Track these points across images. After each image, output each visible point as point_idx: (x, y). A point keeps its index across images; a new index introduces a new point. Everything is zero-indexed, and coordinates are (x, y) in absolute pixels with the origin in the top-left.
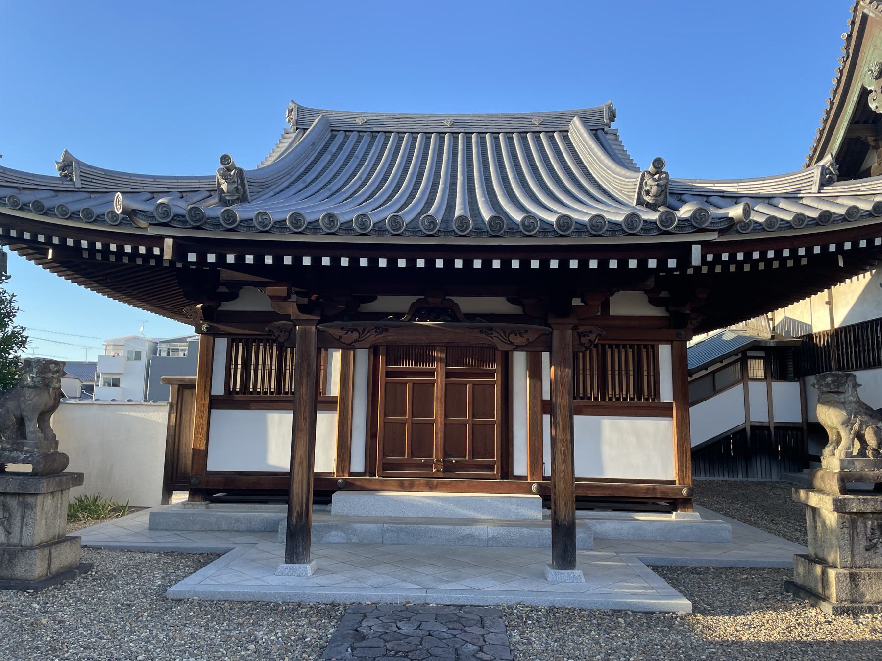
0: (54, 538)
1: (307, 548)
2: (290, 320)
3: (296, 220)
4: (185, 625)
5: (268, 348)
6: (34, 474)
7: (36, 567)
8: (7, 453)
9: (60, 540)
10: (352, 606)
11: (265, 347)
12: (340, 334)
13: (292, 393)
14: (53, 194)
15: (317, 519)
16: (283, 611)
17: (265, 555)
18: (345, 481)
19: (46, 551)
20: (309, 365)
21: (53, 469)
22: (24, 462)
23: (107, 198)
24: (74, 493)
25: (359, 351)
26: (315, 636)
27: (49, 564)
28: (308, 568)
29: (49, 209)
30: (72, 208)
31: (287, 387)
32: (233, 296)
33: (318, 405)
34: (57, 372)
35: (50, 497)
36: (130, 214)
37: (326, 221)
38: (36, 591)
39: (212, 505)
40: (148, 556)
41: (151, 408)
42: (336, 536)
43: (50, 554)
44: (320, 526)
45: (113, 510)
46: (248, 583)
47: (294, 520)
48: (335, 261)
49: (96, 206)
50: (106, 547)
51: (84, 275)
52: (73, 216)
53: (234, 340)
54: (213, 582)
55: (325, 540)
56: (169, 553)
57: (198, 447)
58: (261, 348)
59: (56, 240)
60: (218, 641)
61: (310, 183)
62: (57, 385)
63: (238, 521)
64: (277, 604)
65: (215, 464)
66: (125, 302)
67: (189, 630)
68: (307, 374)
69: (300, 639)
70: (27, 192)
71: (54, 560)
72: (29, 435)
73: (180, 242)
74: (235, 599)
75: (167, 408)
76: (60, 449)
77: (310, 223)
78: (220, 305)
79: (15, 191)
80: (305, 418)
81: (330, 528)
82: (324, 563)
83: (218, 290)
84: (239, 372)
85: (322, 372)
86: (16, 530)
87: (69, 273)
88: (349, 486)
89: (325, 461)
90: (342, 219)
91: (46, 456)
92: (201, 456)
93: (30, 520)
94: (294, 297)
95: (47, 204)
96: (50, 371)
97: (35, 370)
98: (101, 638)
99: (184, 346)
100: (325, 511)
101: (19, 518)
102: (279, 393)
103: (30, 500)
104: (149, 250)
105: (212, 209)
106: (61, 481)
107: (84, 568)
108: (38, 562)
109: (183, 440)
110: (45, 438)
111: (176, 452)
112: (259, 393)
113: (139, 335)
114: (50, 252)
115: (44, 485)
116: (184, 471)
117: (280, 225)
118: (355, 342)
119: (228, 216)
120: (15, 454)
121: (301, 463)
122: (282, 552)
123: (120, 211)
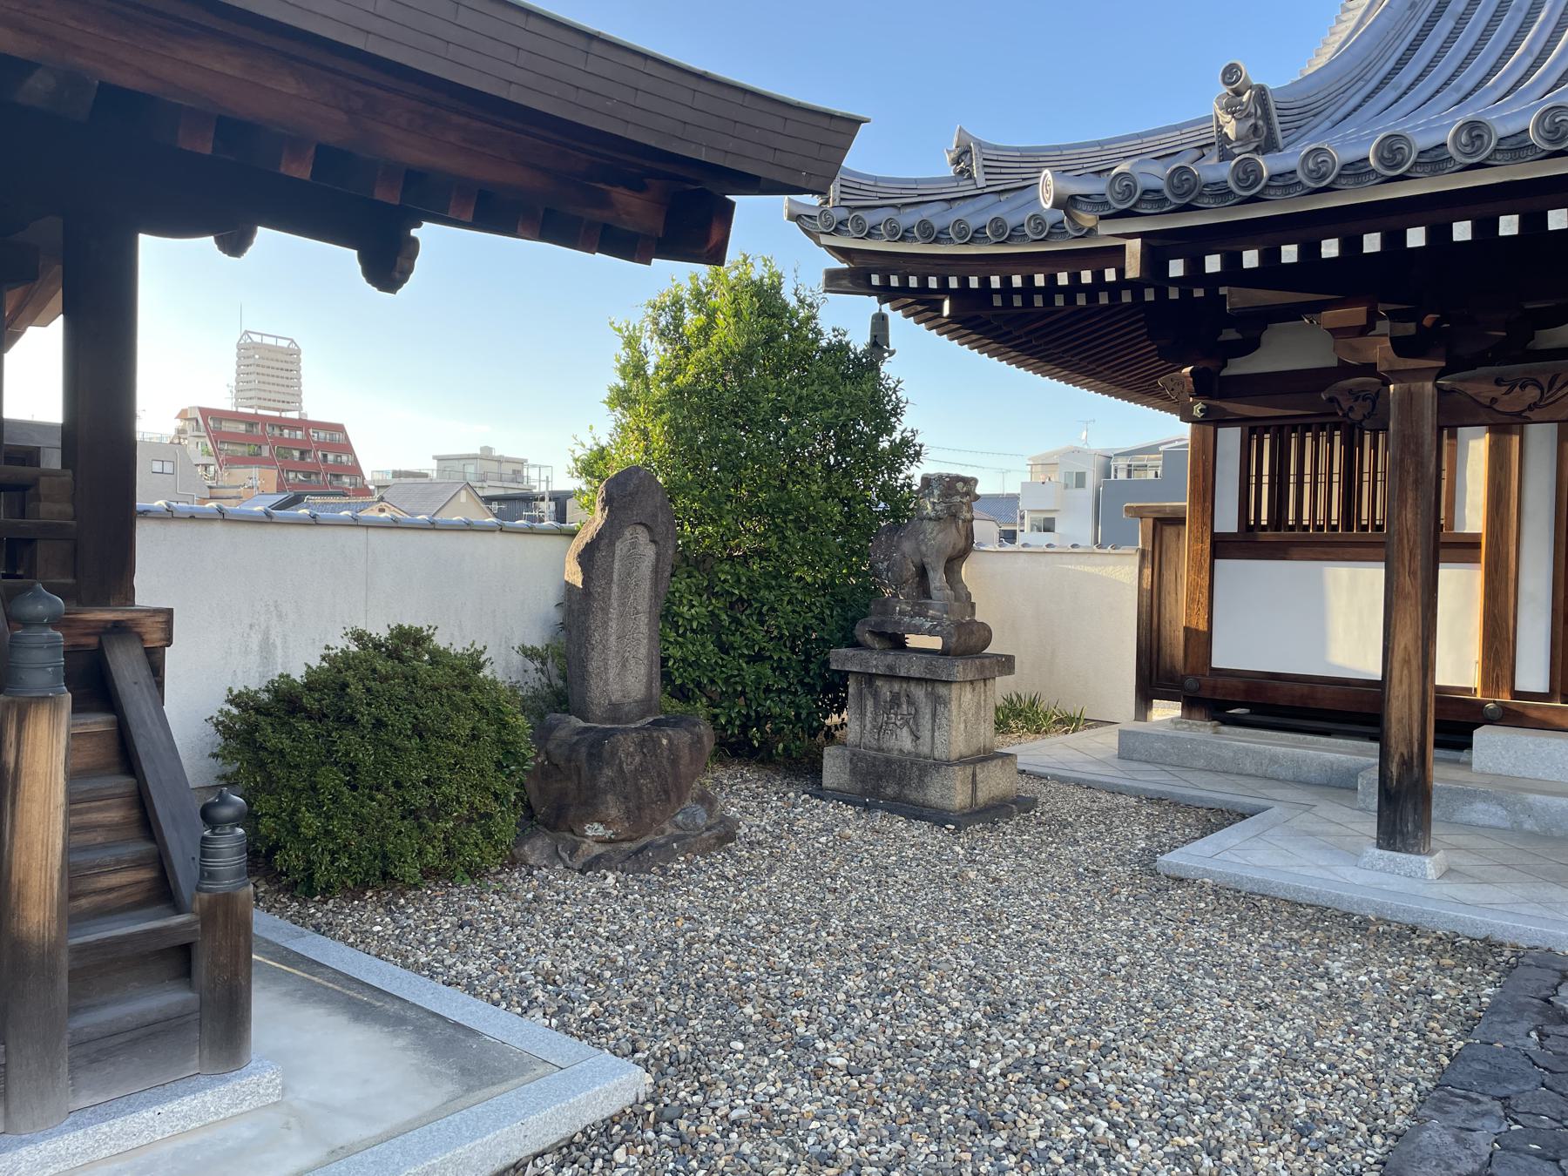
0: (979, 751)
1: (1424, 824)
2: (1378, 375)
3: (1391, 151)
4: (1193, 922)
5: (1323, 440)
6: (944, 652)
7: (954, 792)
8: (907, 619)
9: (986, 756)
10: (1534, 953)
11: (1316, 439)
12: (1493, 394)
13: (1380, 528)
14: (945, 205)
15: (1442, 774)
16: (1379, 936)
17: (1333, 829)
18: (1504, 707)
19: (969, 770)
20: (1420, 465)
21: (970, 646)
22: (930, 633)
23: (1026, 196)
24: (1002, 687)
25: (1532, 430)
26: (1453, 993)
27: (974, 790)
28: (1430, 865)
29: (940, 232)
30: (974, 223)
31: (1364, 515)
32: (1249, 346)
33: (1442, 552)
34: (967, 494)
35: (968, 688)
36: (1067, 203)
37: (1464, 138)
38: (958, 829)
39: (1225, 729)
40: (1121, 800)
41: (1110, 558)
42: (1481, 812)
43: (974, 775)
44: (1450, 790)
45: (1060, 721)
46: (1303, 871)
47: (1394, 769)
48: (1486, 227)
49: (1012, 213)
50: (1054, 777)
51: (996, 339)
52: (977, 236)
53: (1253, 430)
54: (1237, 860)
55: (1457, 817)
56: (1156, 799)
57: (1193, 626)
58: (1308, 441)
59: (953, 283)
60: (1255, 960)
61: (1409, 88)
62: (968, 516)
63: (1274, 760)
64: (1365, 920)
65: (1228, 654)
66: (1060, 379)
67: (1199, 932)
68: (1416, 481)
69: (1419, 992)
70: (908, 210)
71: (980, 785)
72: (934, 593)
73: (1155, 243)
74: (1280, 895)
75: (1137, 558)
76: (978, 618)
77: (1422, 153)
78: (1225, 365)
79: (890, 213)
80: (1412, 573)
81: (1470, 796)
82: (1464, 862)
83: (1221, 338)
84: (1265, 489)
85: (1444, 483)
86: (925, 734)
87: (974, 337)
88: (1511, 717)
89: (1458, 663)
90: (1503, 130)
91: (960, 626)
92: (1200, 641)
93: (944, 721)
94: (1383, 326)
95: (938, 224)
96: (958, 493)
97: (936, 492)
98: (1058, 916)
99: (1156, 461)
100: (1457, 762)
101: (928, 716)
102: (1348, 527)
103: (942, 690)
104: (1098, 275)
105: (1214, 170)
106: (982, 665)
107: (1025, 804)
108: (958, 785)
109: (1167, 614)
110: (957, 599)
111: (1155, 634)
112: (1306, 528)
113: (1080, 445)
114: (947, 304)
115: (960, 670)
116: (1173, 669)
117: (1356, 171)
118: (1530, 408)
119: (1245, 172)
120: (917, 621)
121: (1406, 662)
122: (1371, 827)
123: (1050, 203)
